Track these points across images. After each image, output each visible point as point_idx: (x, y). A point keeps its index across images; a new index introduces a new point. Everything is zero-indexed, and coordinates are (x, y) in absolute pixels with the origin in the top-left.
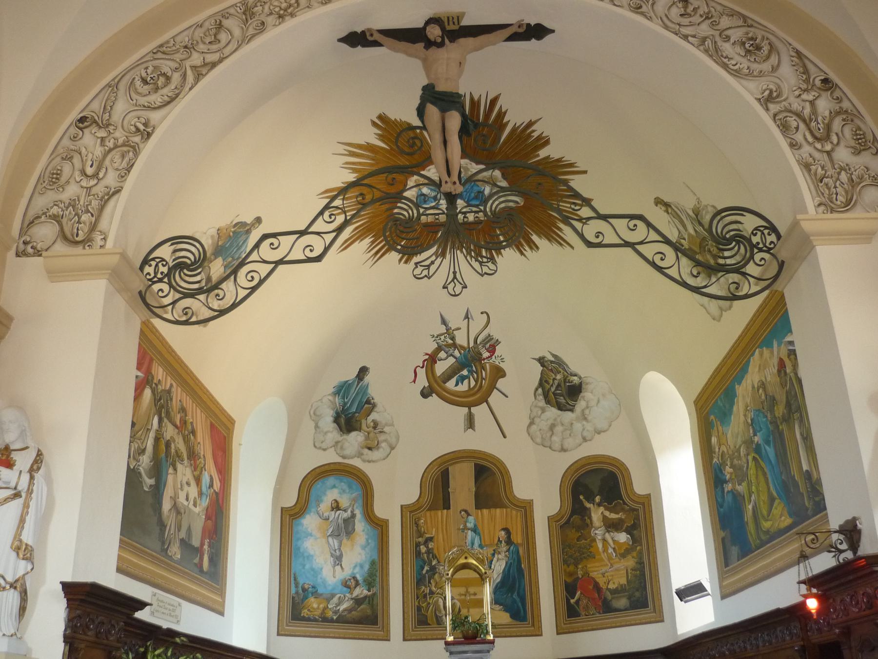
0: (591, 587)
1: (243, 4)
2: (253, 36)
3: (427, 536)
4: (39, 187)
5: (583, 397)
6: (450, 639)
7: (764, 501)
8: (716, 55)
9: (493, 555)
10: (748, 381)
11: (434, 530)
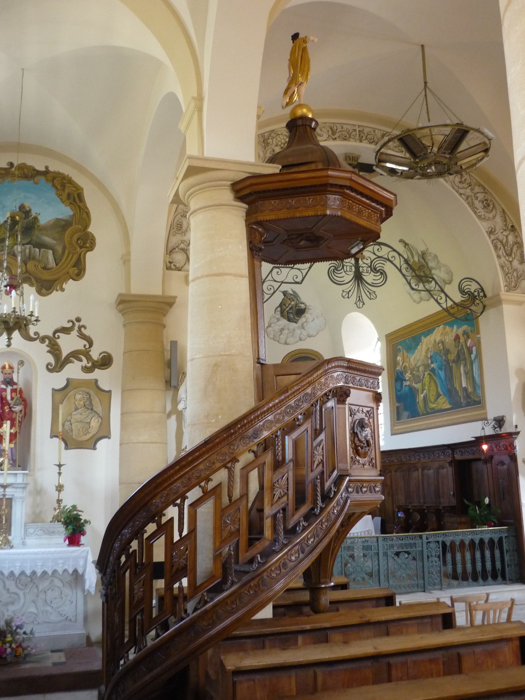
1: (262, 136)
4: (172, 231)
5: (305, 316)
7: (433, 395)
8: (472, 205)
10: (432, 338)
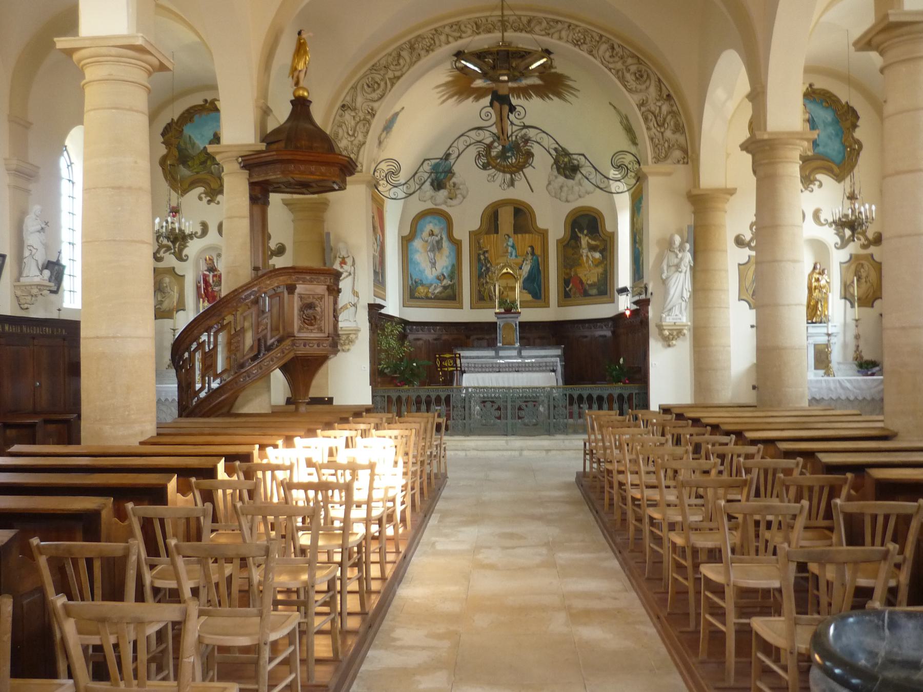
0: (578, 282)
2: (415, 62)
6: (497, 311)
8: (622, 80)
9: (523, 261)
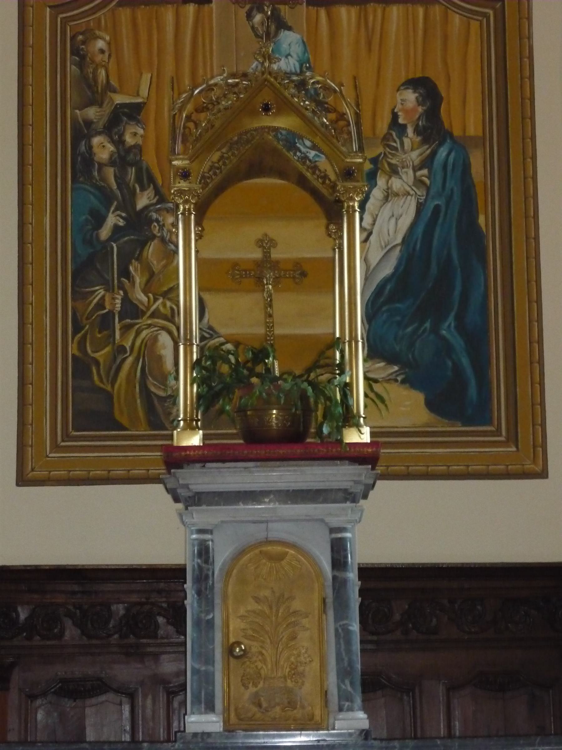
3: (119, 99)
11: (146, 78)
